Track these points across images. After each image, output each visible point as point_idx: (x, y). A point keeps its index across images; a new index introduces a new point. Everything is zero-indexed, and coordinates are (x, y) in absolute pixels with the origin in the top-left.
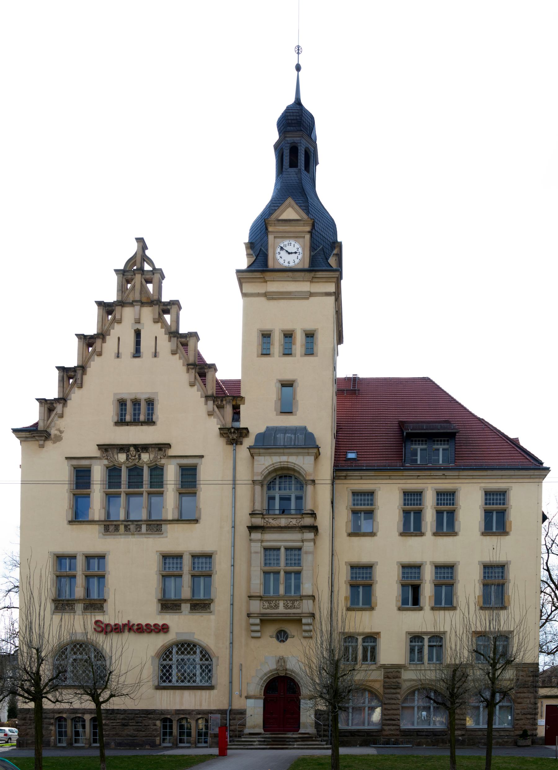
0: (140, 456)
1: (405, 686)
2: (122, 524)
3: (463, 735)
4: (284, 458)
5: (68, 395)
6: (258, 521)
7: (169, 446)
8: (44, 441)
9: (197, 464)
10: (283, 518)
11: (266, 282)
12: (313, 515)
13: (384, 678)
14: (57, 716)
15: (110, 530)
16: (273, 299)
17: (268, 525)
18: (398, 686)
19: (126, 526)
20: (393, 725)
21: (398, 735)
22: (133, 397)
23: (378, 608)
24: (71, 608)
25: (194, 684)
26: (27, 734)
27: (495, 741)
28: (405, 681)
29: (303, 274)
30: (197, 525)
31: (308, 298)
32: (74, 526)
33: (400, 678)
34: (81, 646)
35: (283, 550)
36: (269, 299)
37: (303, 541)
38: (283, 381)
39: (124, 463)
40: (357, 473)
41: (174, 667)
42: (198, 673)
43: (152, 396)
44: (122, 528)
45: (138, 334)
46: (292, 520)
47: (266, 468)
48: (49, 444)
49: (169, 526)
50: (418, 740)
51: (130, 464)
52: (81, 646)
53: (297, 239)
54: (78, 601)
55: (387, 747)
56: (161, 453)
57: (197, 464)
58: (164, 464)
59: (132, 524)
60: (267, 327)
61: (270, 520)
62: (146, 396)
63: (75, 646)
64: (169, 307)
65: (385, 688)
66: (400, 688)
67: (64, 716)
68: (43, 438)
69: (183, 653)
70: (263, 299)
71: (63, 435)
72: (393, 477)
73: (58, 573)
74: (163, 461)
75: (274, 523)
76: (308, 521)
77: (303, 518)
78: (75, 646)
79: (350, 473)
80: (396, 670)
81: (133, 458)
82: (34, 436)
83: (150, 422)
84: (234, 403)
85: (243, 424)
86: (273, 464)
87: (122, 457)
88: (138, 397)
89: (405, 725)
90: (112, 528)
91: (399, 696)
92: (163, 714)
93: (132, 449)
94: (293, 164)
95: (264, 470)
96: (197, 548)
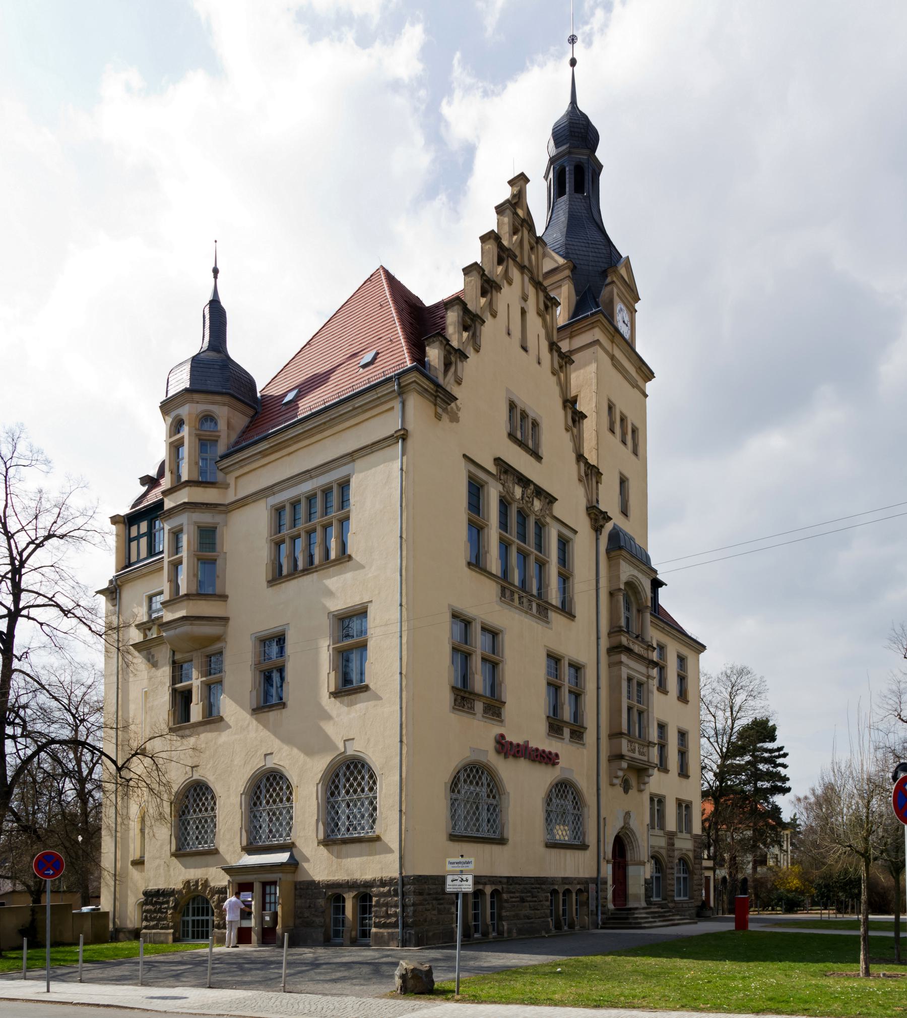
31: (633, 387)
36: (614, 365)
63: (471, 770)
78: (471, 770)
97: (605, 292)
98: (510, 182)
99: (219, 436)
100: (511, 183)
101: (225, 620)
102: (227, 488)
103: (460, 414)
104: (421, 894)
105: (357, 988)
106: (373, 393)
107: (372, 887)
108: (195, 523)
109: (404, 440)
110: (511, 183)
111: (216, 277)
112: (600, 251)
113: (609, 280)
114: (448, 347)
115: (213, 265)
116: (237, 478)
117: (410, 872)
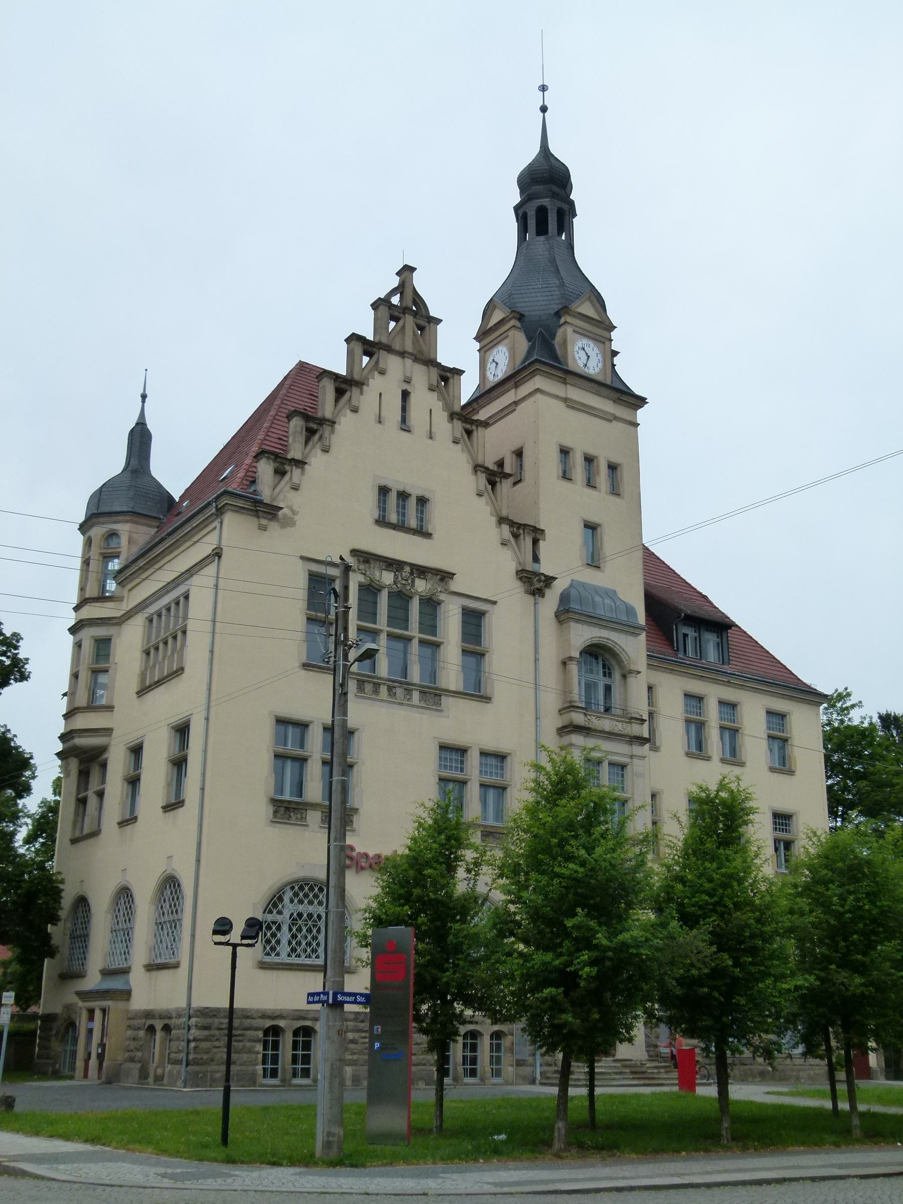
0: (413, 582)
2: (384, 684)
5: (307, 456)
6: (578, 718)
7: (451, 575)
14: (268, 1023)
15: (366, 691)
16: (573, 408)
19: (390, 689)
22: (401, 489)
24: (299, 816)
25: (277, 960)
26: (212, 1060)
30: (489, 705)
31: (610, 421)
32: (311, 673)
34: (311, 889)
35: (605, 765)
36: (568, 406)
37: (632, 757)
39: (389, 586)
41: (285, 928)
42: (284, 941)
43: (427, 495)
44: (384, 690)
45: (405, 395)
46: (617, 723)
48: (274, 526)
49: (451, 699)
52: (311, 889)
54: (314, 806)
57: (487, 612)
58: (443, 601)
59: (399, 687)
60: (568, 443)
62: (420, 493)
63: (301, 888)
64: (449, 375)
67: (282, 1023)
69: (301, 902)
70: (561, 405)
71: (296, 518)
73: (281, 749)
74: (442, 597)
77: (631, 723)
78: (301, 888)
81: (404, 582)
82: (257, 511)
83: (422, 532)
85: (545, 568)
87: (387, 578)
88: (409, 490)
90: (368, 687)
92: (248, 1017)
93: (407, 569)
94: (542, 230)
96: (491, 745)
97: (560, 333)
98: (397, 274)
99: (120, 552)
100: (398, 274)
101: (108, 731)
102: (122, 601)
103: (296, 518)
104: (206, 1028)
105: (377, 1169)
106: (201, 515)
107: (170, 1018)
108: (92, 637)
109: (220, 557)
110: (398, 274)
111: (143, 402)
112: (553, 293)
113: (562, 320)
114: (279, 460)
115: (142, 392)
116: (130, 590)
117: (194, 1005)
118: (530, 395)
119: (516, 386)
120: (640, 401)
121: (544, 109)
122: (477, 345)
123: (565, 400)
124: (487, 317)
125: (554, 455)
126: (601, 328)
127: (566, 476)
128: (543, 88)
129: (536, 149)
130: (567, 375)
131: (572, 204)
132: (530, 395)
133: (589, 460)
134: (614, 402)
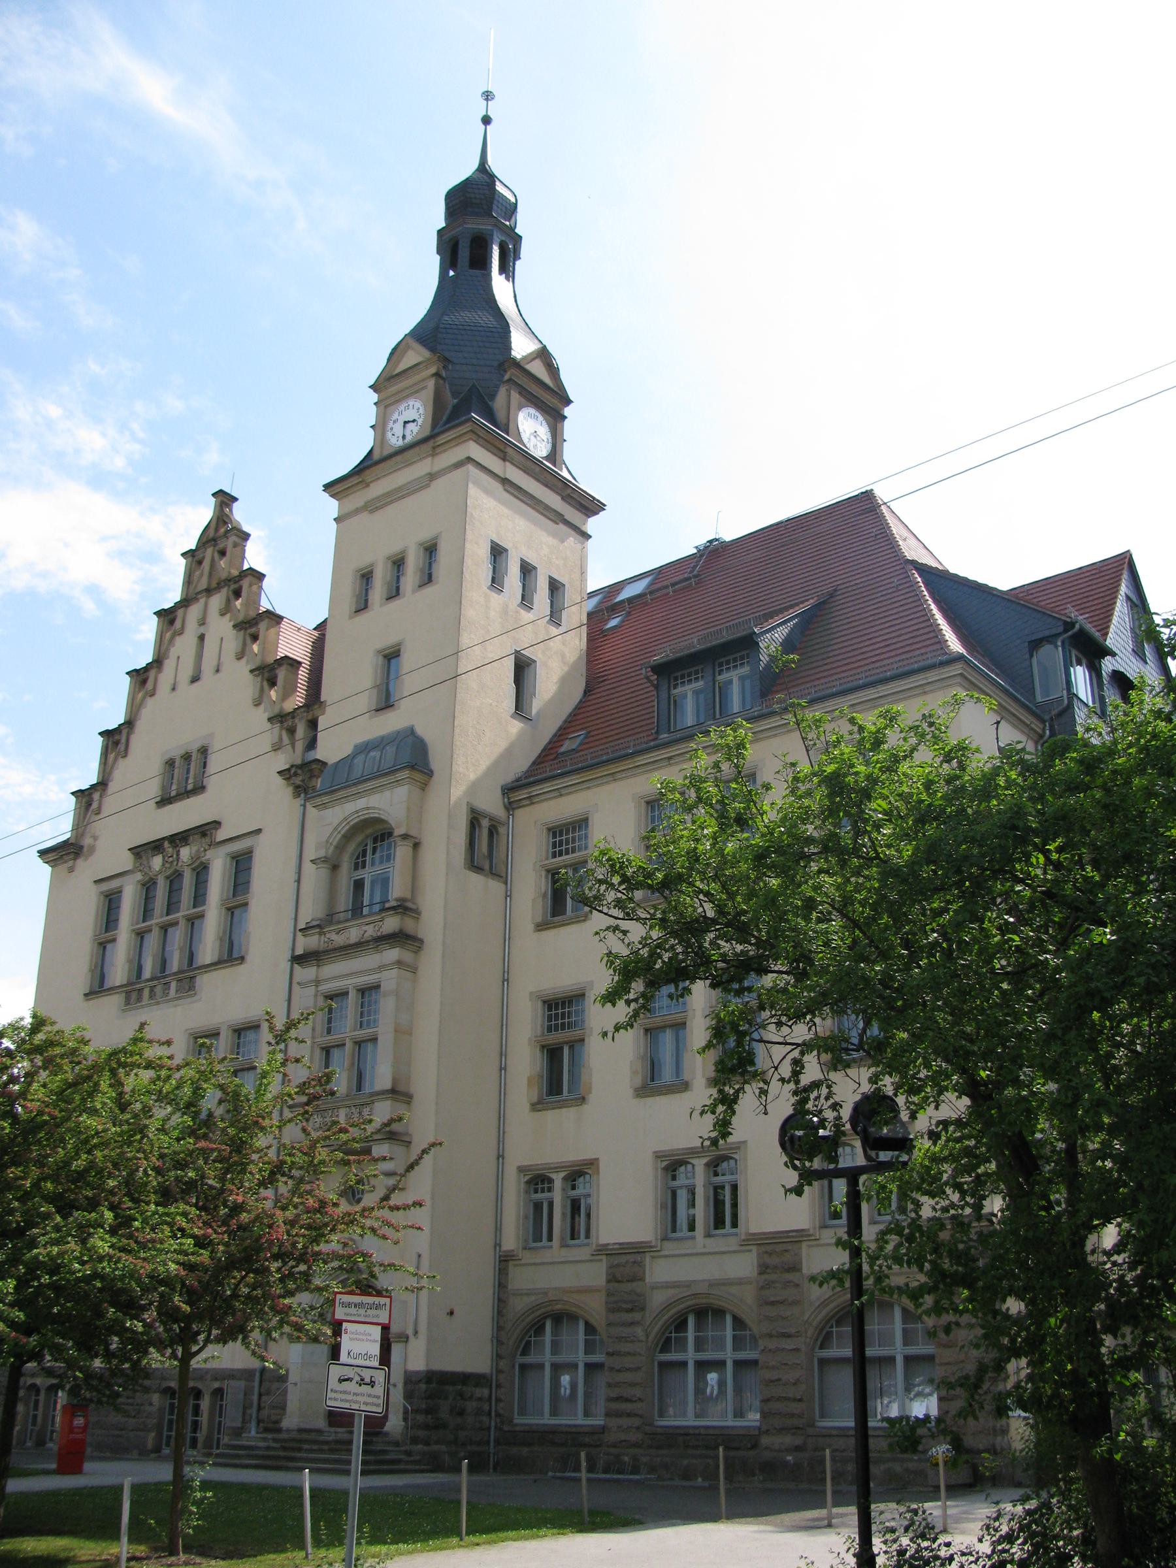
1: (658, 1299)
3: (798, 1449)
4: (361, 803)
7: (217, 824)
8: (75, 859)
9: (252, 847)
10: (352, 926)
11: (368, 485)
12: (404, 908)
13: (609, 1281)
16: (377, 509)
17: (331, 947)
18: (637, 1305)
20: (629, 1415)
21: (636, 1445)
23: (592, 1098)
27: (882, 1467)
28: (654, 1287)
29: (416, 450)
31: (428, 486)
33: (642, 1279)
36: (371, 512)
38: (385, 650)
39: (160, 872)
40: (547, 787)
47: (336, 829)
48: (80, 862)
49: (206, 976)
50: (685, 1462)
51: (169, 872)
53: (468, 373)
55: (617, 1481)
56: (208, 840)
57: (252, 847)
61: (334, 936)
62: (197, 745)
65: (612, 1309)
66: (643, 1309)
68: (72, 856)
70: (365, 516)
72: (619, 776)
75: (339, 940)
76: (391, 924)
79: (536, 790)
80: (631, 1258)
84: (310, 717)
86: (346, 819)
89: (684, 1416)
91: (639, 1331)
95: (332, 834)
118: (458, 465)
119: (434, 452)
120: (591, 507)
121: (486, 120)
122: (375, 397)
123: (505, 481)
124: (394, 358)
125: (484, 552)
126: (552, 402)
127: (496, 582)
128: (488, 96)
129: (474, 165)
130: (507, 449)
131: (519, 238)
132: (458, 465)
133: (527, 570)
134: (563, 499)
